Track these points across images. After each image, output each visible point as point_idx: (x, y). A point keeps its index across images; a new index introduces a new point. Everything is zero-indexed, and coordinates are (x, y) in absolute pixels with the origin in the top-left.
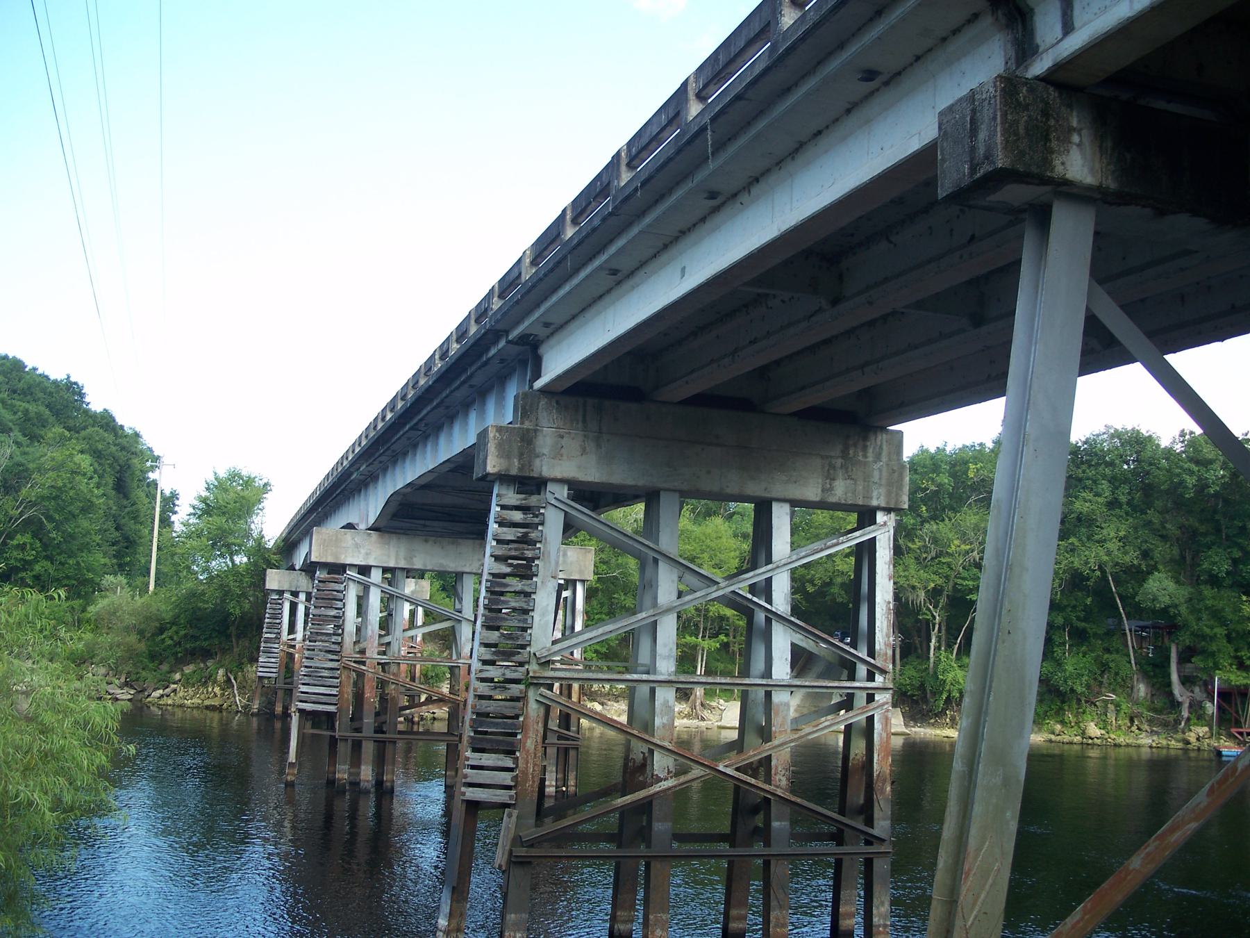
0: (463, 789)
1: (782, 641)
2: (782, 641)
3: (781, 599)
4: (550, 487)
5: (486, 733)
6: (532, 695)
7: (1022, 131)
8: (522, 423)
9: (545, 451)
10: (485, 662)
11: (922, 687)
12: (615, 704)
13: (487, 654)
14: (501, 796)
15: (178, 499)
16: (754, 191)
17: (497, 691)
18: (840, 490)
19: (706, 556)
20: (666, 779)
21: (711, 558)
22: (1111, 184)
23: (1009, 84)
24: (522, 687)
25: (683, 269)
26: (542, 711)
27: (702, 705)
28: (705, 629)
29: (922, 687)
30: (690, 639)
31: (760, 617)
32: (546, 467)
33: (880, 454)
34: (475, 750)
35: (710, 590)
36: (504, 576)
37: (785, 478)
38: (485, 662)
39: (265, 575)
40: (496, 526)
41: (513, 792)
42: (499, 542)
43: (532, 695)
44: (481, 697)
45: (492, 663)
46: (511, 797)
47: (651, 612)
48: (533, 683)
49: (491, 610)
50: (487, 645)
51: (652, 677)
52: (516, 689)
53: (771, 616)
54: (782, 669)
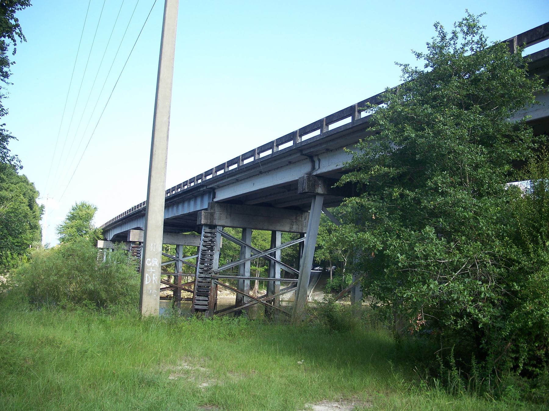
0: (195, 306)
1: (278, 269)
2: (278, 269)
3: (278, 258)
4: (218, 227)
5: (200, 291)
6: (213, 281)
7: (310, 185)
8: (211, 210)
9: (217, 218)
10: (200, 273)
11: (340, 286)
12: (225, 291)
13: (201, 271)
14: (205, 308)
15: (44, 208)
16: (269, 173)
17: (204, 280)
18: (295, 228)
19: (260, 236)
20: (247, 304)
21: (262, 237)
22: (326, 193)
23: (309, 174)
24: (210, 279)
25: (254, 184)
26: (215, 285)
27: (258, 292)
28: (259, 264)
29: (340, 286)
30: (253, 267)
31: (273, 262)
32: (217, 222)
33: (306, 218)
34: (198, 296)
35: (259, 254)
36: (205, 250)
37: (279, 225)
38: (200, 273)
39: (97, 242)
40: (203, 237)
41: (208, 306)
42: (204, 241)
43: (213, 281)
44: (199, 282)
45: (202, 273)
46: (207, 308)
47: (244, 260)
48: (213, 278)
49: (202, 259)
50: (201, 268)
51: (244, 277)
52: (209, 280)
53: (276, 262)
54: (278, 276)
